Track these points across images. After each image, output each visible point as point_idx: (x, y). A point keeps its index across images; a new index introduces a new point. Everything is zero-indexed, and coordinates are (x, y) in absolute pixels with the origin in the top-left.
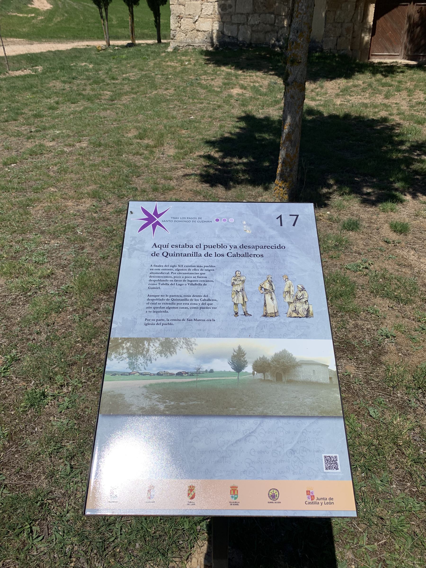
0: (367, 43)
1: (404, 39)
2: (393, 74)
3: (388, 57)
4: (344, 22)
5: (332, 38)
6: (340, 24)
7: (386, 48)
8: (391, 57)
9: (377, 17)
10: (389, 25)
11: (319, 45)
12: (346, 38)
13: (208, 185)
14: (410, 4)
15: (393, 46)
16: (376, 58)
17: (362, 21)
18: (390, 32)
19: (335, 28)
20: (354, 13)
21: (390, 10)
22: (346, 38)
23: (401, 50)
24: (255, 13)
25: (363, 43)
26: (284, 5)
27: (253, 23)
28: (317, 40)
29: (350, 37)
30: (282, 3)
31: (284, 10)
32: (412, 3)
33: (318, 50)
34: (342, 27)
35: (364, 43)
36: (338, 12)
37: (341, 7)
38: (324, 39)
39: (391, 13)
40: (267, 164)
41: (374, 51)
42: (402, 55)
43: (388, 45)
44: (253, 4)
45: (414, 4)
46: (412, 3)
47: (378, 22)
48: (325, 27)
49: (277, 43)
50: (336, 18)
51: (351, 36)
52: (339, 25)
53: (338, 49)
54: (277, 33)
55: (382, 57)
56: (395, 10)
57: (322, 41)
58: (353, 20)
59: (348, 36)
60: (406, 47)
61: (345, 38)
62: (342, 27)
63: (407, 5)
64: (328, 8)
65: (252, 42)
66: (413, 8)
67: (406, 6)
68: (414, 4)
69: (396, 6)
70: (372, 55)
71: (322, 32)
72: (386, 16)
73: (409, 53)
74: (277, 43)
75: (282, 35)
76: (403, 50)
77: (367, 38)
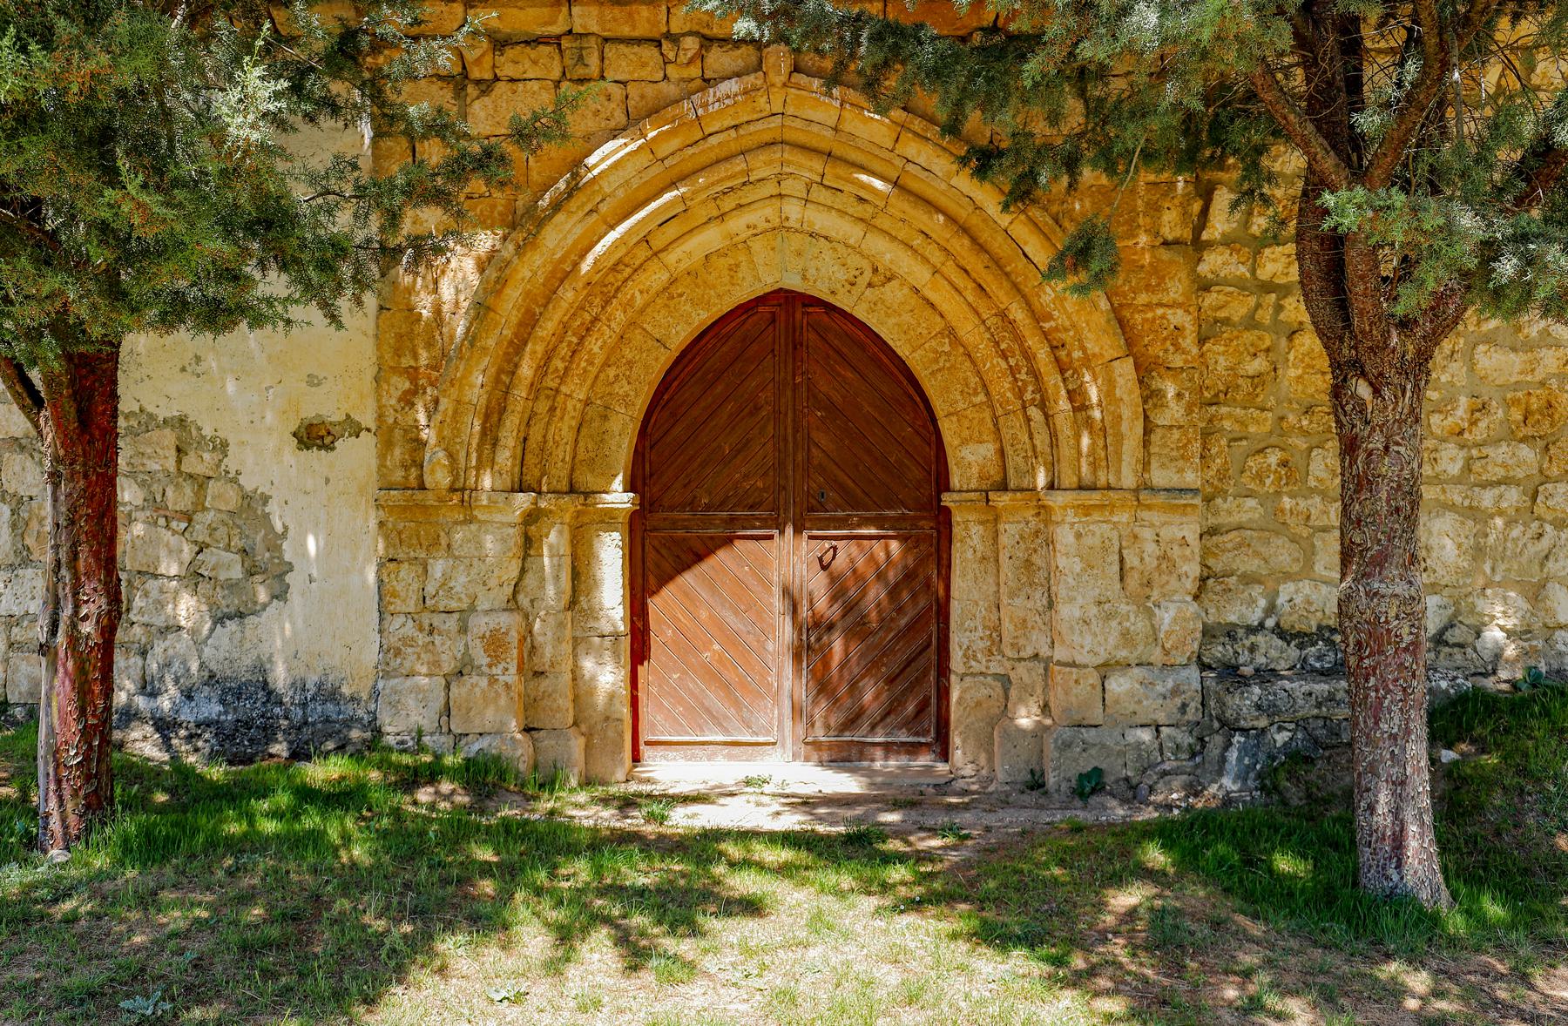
0: (612, 696)
1: (788, 681)
2: (695, 932)
3: (726, 750)
4: (472, 608)
5: (424, 681)
6: (456, 616)
7: (708, 711)
8: (736, 750)
9: (642, 587)
10: (704, 615)
11: (360, 713)
12: (493, 680)
13: (1020, 961)
14: (782, 533)
15: (737, 705)
16: (671, 754)
17: (573, 603)
18: (716, 647)
19: (431, 633)
20: (523, 571)
21: (699, 558)
22: (493, 680)
23: (776, 718)
24: (26, 562)
25: (591, 691)
26: (174, 532)
27: (17, 611)
28: (346, 690)
29: (512, 677)
30: (162, 521)
31: (174, 552)
32: (789, 530)
33: (355, 734)
34: (463, 630)
35: (601, 699)
36: (438, 568)
37: (449, 546)
38: (380, 685)
39: (705, 567)
40: (1284, 863)
41: (655, 723)
42: (789, 742)
43: (714, 699)
44: (14, 526)
45: (798, 531)
46: (789, 530)
47: (655, 605)
48: (380, 631)
49: (141, 702)
50: (430, 589)
51: (513, 670)
52: (452, 623)
53: (456, 730)
54: (143, 653)
55: (697, 750)
56: (722, 555)
57: (375, 694)
58: (524, 600)
59: (497, 670)
60: (797, 711)
61: (484, 682)
62: (463, 630)
63: (771, 537)
64: (386, 548)
65: (12, 699)
66: (796, 549)
67: (764, 543)
68: (798, 531)
69: (728, 541)
70: (648, 743)
71: (371, 655)
72: (688, 579)
73: (819, 733)
74: (141, 702)
75: (168, 665)
76: (788, 723)
77: (607, 676)
